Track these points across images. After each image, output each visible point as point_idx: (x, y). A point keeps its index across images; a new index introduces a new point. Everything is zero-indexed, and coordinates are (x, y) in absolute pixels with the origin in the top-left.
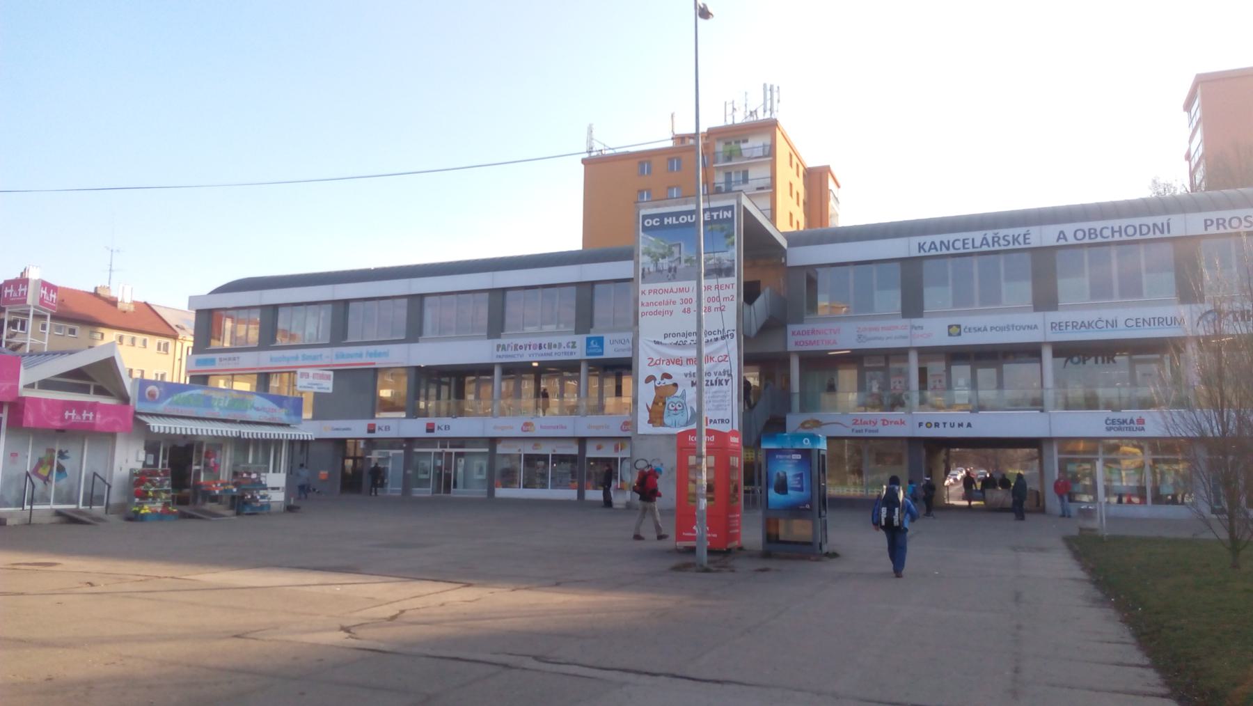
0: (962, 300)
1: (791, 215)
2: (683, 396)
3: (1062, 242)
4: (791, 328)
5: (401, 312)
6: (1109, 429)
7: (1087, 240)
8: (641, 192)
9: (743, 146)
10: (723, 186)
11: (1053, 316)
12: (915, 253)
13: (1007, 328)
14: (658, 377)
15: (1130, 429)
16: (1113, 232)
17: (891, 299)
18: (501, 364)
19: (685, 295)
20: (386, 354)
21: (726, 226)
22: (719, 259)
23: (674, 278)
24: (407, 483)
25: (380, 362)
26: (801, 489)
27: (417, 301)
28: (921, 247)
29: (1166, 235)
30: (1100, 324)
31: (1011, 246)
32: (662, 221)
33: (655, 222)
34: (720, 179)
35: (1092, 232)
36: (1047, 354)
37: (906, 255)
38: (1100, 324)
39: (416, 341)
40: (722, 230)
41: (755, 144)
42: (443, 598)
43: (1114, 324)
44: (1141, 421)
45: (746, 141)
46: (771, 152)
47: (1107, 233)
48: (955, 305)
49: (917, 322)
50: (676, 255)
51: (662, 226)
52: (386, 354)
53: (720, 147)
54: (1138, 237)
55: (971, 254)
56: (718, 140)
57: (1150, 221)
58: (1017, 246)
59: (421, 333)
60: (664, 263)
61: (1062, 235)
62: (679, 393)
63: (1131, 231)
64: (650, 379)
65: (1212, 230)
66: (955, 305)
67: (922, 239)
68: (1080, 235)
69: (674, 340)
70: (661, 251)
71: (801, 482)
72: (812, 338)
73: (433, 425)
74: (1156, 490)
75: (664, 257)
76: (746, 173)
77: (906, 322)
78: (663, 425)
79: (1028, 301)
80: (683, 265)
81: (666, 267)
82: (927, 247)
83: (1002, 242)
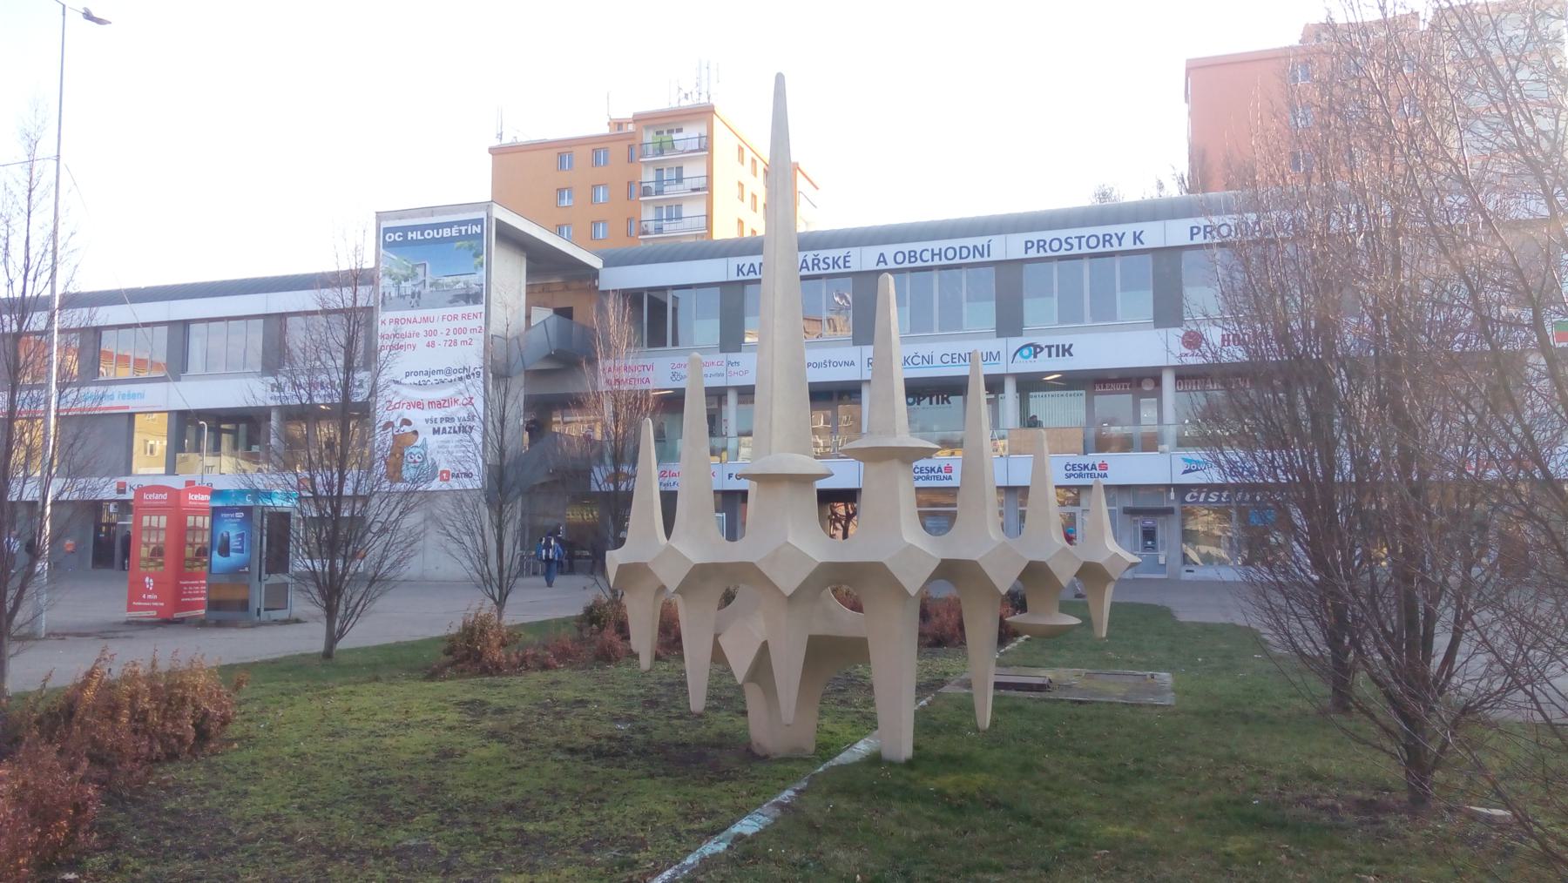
0: (1070, 315)
1: (740, 222)
2: (424, 446)
3: (882, 266)
5: (256, 336)
6: (1068, 477)
7: (906, 265)
8: (560, 191)
9: (675, 136)
10: (652, 185)
12: (733, 277)
13: (825, 364)
14: (397, 424)
16: (933, 255)
17: (983, 313)
19: (429, 326)
20: (142, 396)
21: (474, 243)
22: (466, 283)
23: (418, 306)
25: (133, 405)
26: (241, 551)
27: (181, 328)
28: (739, 270)
29: (986, 259)
30: (916, 360)
31: (831, 271)
32: (405, 236)
33: (396, 237)
34: (649, 176)
35: (912, 255)
36: (1168, 380)
37: (724, 279)
38: (916, 360)
39: (178, 379)
40: (471, 248)
41: (691, 133)
43: (929, 360)
44: (1104, 466)
45: (680, 130)
46: (706, 146)
47: (927, 256)
48: (1061, 321)
49: (733, 357)
50: (421, 278)
51: (406, 243)
52: (142, 396)
53: (649, 137)
54: (957, 261)
55: (1080, 257)
56: (648, 128)
57: (970, 242)
58: (837, 270)
60: (407, 287)
61: (882, 258)
62: (419, 443)
63: (950, 254)
65: (1032, 253)
66: (1061, 321)
67: (740, 260)
68: (900, 258)
69: (416, 379)
70: (404, 272)
71: (242, 543)
72: (645, 374)
73: (124, 484)
75: (406, 280)
76: (680, 169)
77: (722, 357)
80: (428, 289)
81: (409, 292)
82: (745, 270)
83: (822, 265)
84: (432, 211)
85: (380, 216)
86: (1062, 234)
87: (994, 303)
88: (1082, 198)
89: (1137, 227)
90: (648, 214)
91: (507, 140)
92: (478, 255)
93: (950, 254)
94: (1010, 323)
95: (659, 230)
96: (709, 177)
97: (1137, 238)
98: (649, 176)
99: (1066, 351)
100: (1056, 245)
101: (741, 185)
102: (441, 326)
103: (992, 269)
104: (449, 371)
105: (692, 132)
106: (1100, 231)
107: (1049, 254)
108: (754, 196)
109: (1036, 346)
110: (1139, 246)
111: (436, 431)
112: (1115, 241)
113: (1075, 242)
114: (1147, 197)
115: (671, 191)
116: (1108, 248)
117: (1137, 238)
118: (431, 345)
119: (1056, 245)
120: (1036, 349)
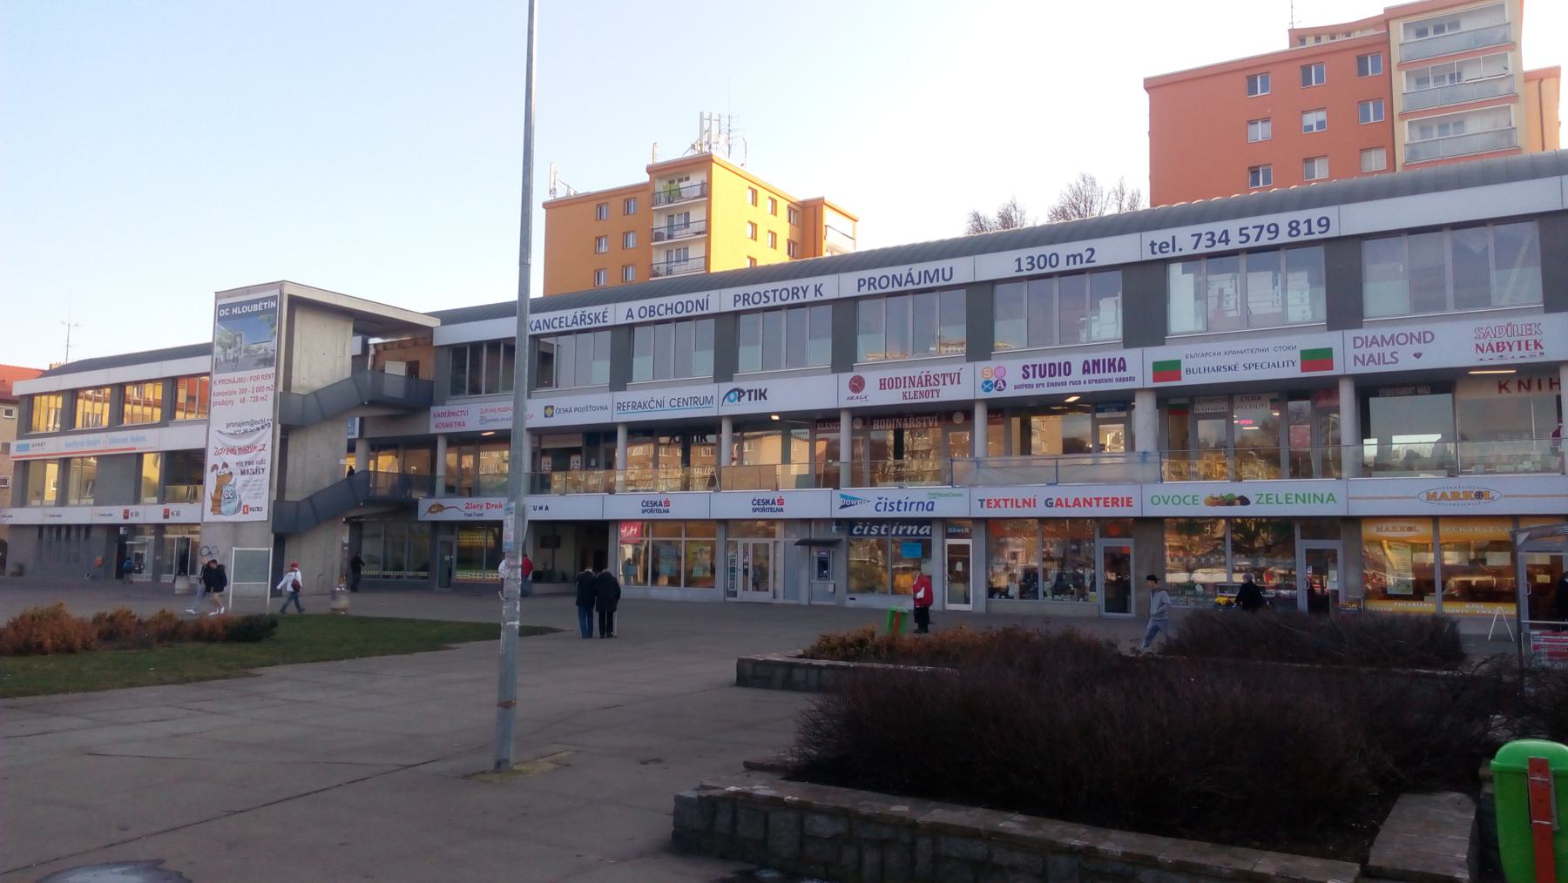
4: (434, 409)
9: (682, 185)
11: (621, 397)
15: (772, 510)
18: (987, 401)
19: (242, 385)
24: (158, 569)
37: (971, 280)
42: (895, 808)
46: (706, 191)
47: (662, 310)
54: (684, 314)
55: (1235, 253)
56: (661, 178)
59: (630, 379)
61: (630, 314)
64: (215, 467)
65: (865, 291)
69: (231, 430)
74: (689, 572)
76: (687, 214)
78: (220, 513)
79: (1537, 300)
84: (247, 290)
85: (218, 295)
86: (762, 288)
87: (830, 340)
88: (958, 229)
89: (817, 280)
90: (659, 258)
91: (561, 194)
92: (273, 326)
93: (679, 308)
94: (725, 368)
95: (669, 272)
96: (708, 221)
97: (817, 290)
98: (660, 223)
99: (762, 395)
100: (757, 298)
101: (754, 225)
102: (249, 385)
103: (830, 307)
104: (252, 423)
105: (697, 179)
106: (790, 284)
107: (879, 291)
108: (774, 235)
109: (740, 391)
110: (819, 298)
111: (243, 473)
112: (801, 293)
113: (771, 295)
114: (1039, 224)
115: (681, 235)
116: (796, 301)
117: (817, 290)
118: (243, 401)
119: (757, 298)
120: (740, 393)
